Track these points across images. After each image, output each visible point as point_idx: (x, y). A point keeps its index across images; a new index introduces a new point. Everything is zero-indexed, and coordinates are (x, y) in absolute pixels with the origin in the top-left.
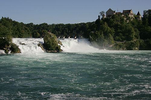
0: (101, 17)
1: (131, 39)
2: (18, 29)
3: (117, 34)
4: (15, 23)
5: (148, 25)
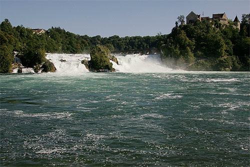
0: (179, 24)
1: (220, 55)
2: (71, 43)
3: (198, 47)
4: (69, 35)
5: (246, 36)
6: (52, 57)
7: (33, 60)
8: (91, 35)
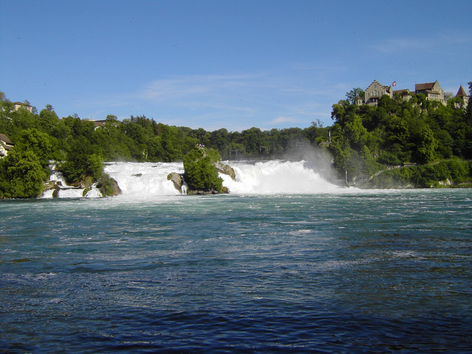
7: (81, 170)
8: (210, 128)
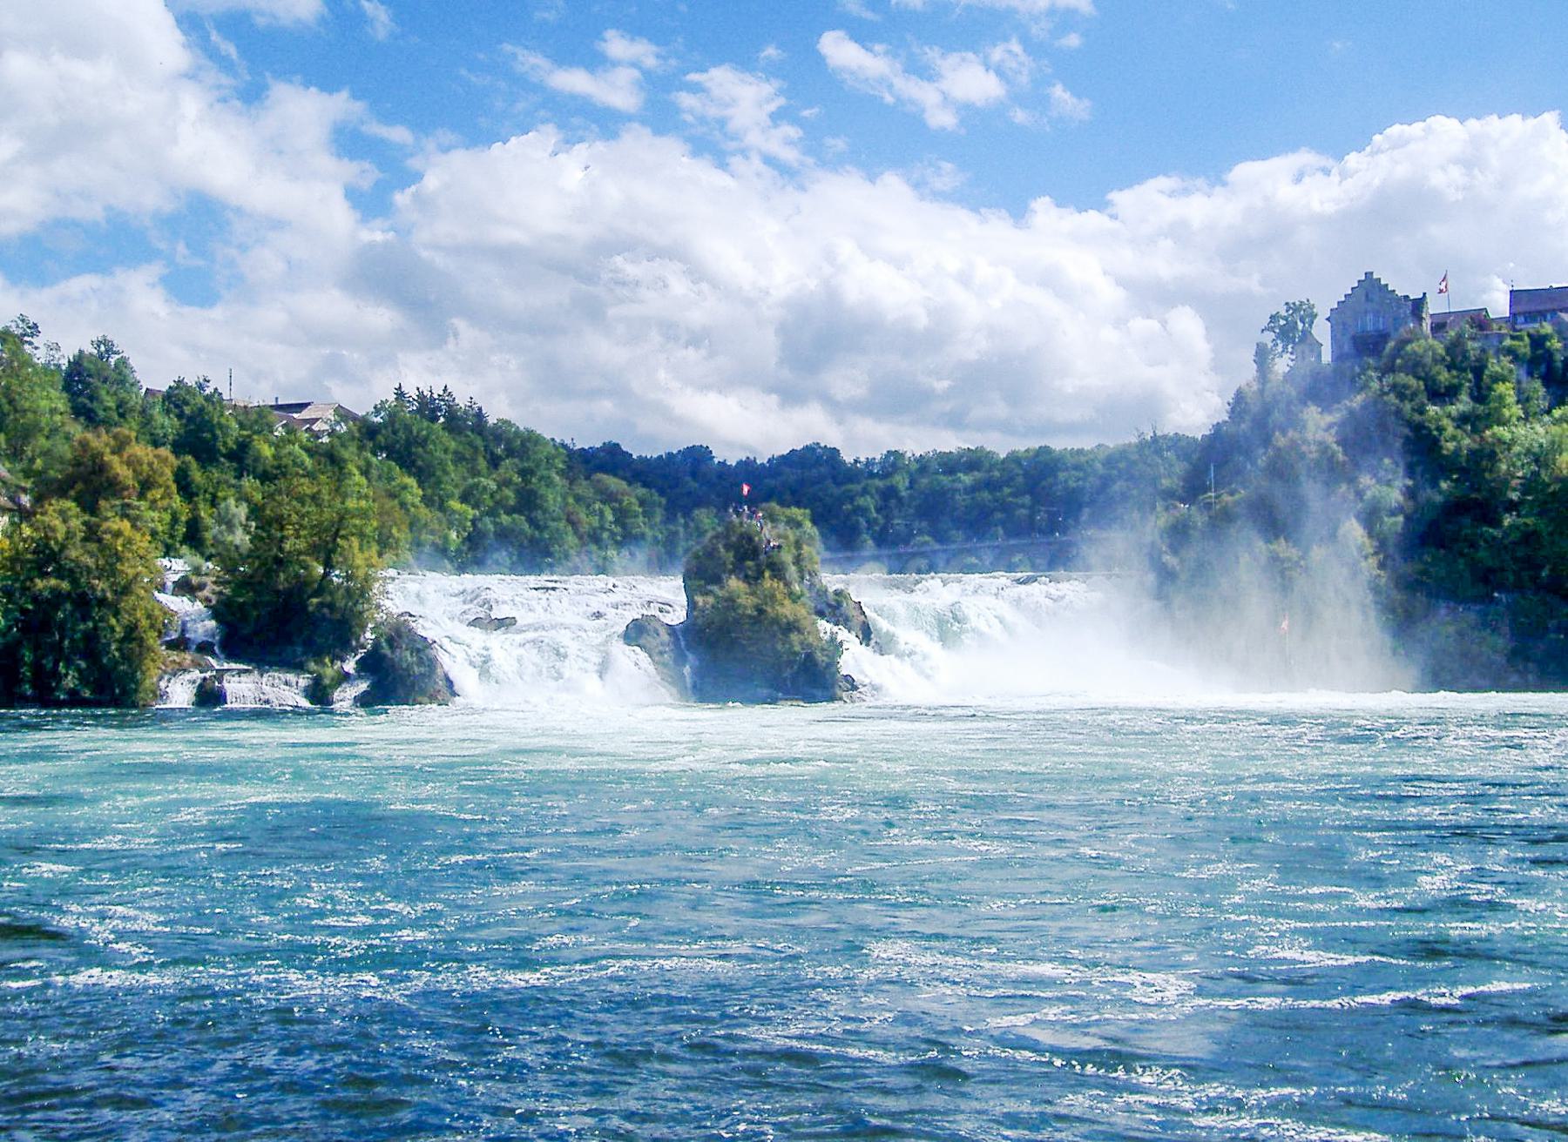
0: (1282, 365)
2: (528, 502)
6: (418, 596)
